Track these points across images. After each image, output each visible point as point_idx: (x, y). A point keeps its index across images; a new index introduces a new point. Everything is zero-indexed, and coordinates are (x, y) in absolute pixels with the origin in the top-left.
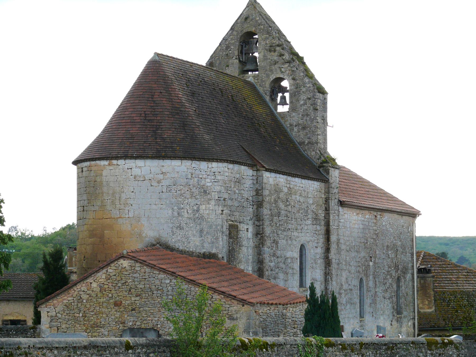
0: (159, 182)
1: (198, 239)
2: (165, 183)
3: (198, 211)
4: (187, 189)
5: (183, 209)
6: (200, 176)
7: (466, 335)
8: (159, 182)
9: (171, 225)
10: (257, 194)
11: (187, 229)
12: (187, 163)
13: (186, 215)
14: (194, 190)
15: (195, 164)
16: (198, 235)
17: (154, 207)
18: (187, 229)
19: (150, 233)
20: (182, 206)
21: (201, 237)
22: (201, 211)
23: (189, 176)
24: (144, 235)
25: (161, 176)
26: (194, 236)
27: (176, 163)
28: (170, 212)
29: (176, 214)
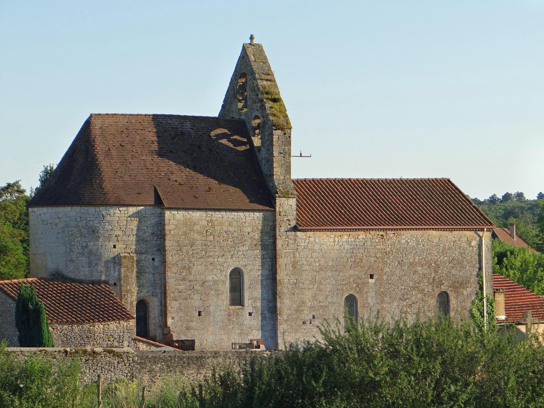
0: (56, 225)
1: (87, 269)
2: (61, 225)
3: (87, 246)
4: (76, 230)
5: (74, 246)
6: (88, 219)
7: (185, 394)
8: (56, 225)
9: (65, 259)
10: (461, 284)
11: (77, 262)
12: (77, 209)
13: (77, 251)
14: (83, 230)
15: (84, 209)
16: (87, 266)
17: (54, 244)
18: (77, 262)
19: (51, 266)
20: (73, 243)
21: (90, 267)
22: (90, 247)
23: (79, 219)
24: (48, 267)
25: (57, 221)
26: (83, 267)
27: (68, 209)
28: (64, 248)
29: (68, 250)
